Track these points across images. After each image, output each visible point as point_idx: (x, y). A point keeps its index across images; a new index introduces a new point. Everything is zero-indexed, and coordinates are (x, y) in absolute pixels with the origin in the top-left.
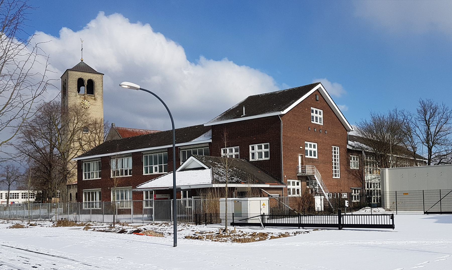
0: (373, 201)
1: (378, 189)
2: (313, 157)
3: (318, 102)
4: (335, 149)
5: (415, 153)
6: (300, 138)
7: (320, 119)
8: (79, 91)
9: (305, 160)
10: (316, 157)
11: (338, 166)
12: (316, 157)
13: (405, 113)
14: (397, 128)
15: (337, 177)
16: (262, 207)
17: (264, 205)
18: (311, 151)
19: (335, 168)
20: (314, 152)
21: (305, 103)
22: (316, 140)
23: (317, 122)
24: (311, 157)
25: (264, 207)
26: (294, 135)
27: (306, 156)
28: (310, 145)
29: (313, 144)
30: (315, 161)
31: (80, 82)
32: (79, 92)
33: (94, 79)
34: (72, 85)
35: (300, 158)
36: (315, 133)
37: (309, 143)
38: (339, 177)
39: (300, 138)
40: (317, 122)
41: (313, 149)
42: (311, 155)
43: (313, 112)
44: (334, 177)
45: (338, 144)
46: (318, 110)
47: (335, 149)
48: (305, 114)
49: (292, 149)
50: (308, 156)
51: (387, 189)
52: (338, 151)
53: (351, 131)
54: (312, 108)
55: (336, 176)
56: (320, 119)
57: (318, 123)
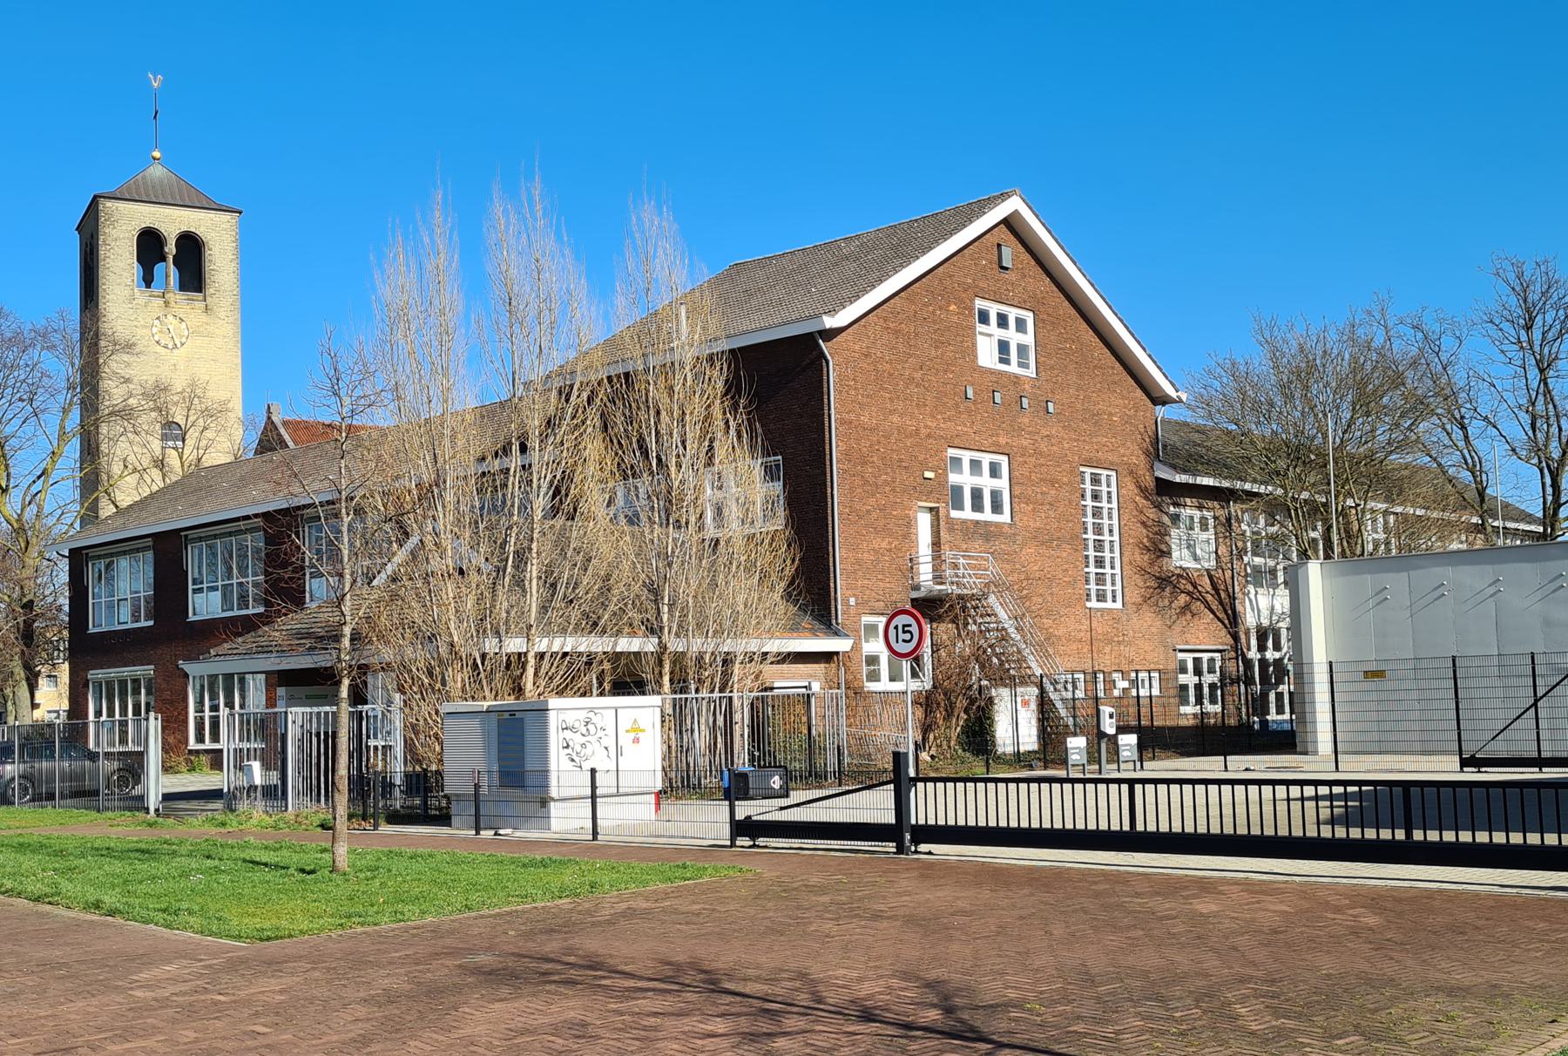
0: (1273, 709)
1: (1271, 655)
2: (987, 515)
3: (1011, 276)
4: (1096, 480)
5: (1481, 494)
6: (924, 431)
7: (1022, 349)
8: (148, 280)
9: (951, 530)
10: (1005, 517)
11: (1111, 554)
12: (1005, 517)
13: (1432, 327)
14: (1399, 389)
15: (1109, 605)
16: (625, 739)
17: (636, 729)
18: (977, 494)
19: (1100, 562)
20: (996, 496)
21: (948, 282)
22: (1002, 440)
23: (1026, 366)
24: (977, 516)
25: (636, 740)
26: (895, 419)
27: (954, 514)
28: (976, 466)
29: (986, 459)
30: (1001, 534)
31: (149, 245)
32: (148, 285)
33: (201, 232)
34: (119, 260)
35: (924, 522)
36: (995, 408)
37: (967, 456)
38: (1119, 605)
39: (924, 431)
40: (1026, 366)
41: (986, 483)
42: (977, 506)
43: (984, 318)
44: (1093, 604)
45: (1111, 457)
46: (1013, 313)
47: (1096, 480)
48: (948, 329)
49: (886, 483)
50: (967, 514)
51: (1319, 653)
52: (1114, 489)
53: (1175, 401)
54: (980, 304)
55: (1101, 597)
56: (1022, 349)
57: (1013, 368)
